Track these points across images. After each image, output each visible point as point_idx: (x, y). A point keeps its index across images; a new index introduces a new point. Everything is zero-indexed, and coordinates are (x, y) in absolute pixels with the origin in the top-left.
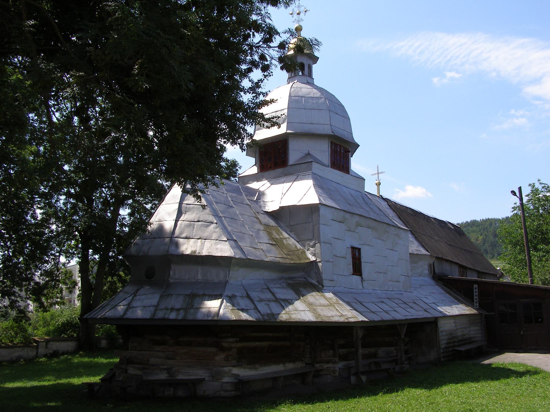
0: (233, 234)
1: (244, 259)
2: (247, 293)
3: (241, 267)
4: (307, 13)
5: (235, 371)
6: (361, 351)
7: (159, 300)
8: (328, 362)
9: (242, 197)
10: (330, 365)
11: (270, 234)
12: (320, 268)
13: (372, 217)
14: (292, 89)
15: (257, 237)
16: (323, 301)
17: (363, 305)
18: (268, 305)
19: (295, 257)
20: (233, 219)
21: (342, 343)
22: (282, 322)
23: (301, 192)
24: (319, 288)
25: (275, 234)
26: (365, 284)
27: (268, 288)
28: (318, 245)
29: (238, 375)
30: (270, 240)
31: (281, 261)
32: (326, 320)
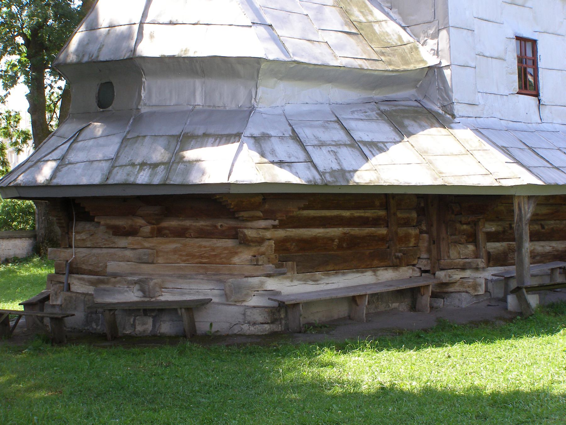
0: (266, 13)
1: (285, 62)
2: (293, 131)
3: (281, 79)
5: (272, 284)
6: (527, 246)
7: (120, 147)
8: (463, 268)
10: (468, 273)
15: (317, 20)
17: (538, 154)
18: (335, 153)
19: (396, 59)
21: (493, 229)
22: (358, 186)
24: (443, 118)
26: (545, 112)
27: (338, 121)
28: (443, 33)
29: (278, 293)
30: (346, 24)
31: (366, 65)
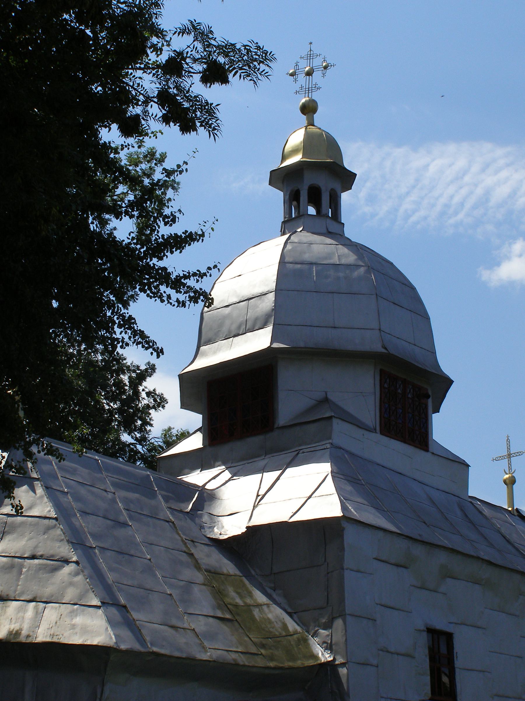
0: (120, 590)
9: (153, 502)
11: (219, 594)
12: (344, 680)
13: (482, 555)
14: (289, 247)
20: (124, 554)
23: (303, 492)
25: (232, 594)
30: (219, 607)
31: (242, 660)
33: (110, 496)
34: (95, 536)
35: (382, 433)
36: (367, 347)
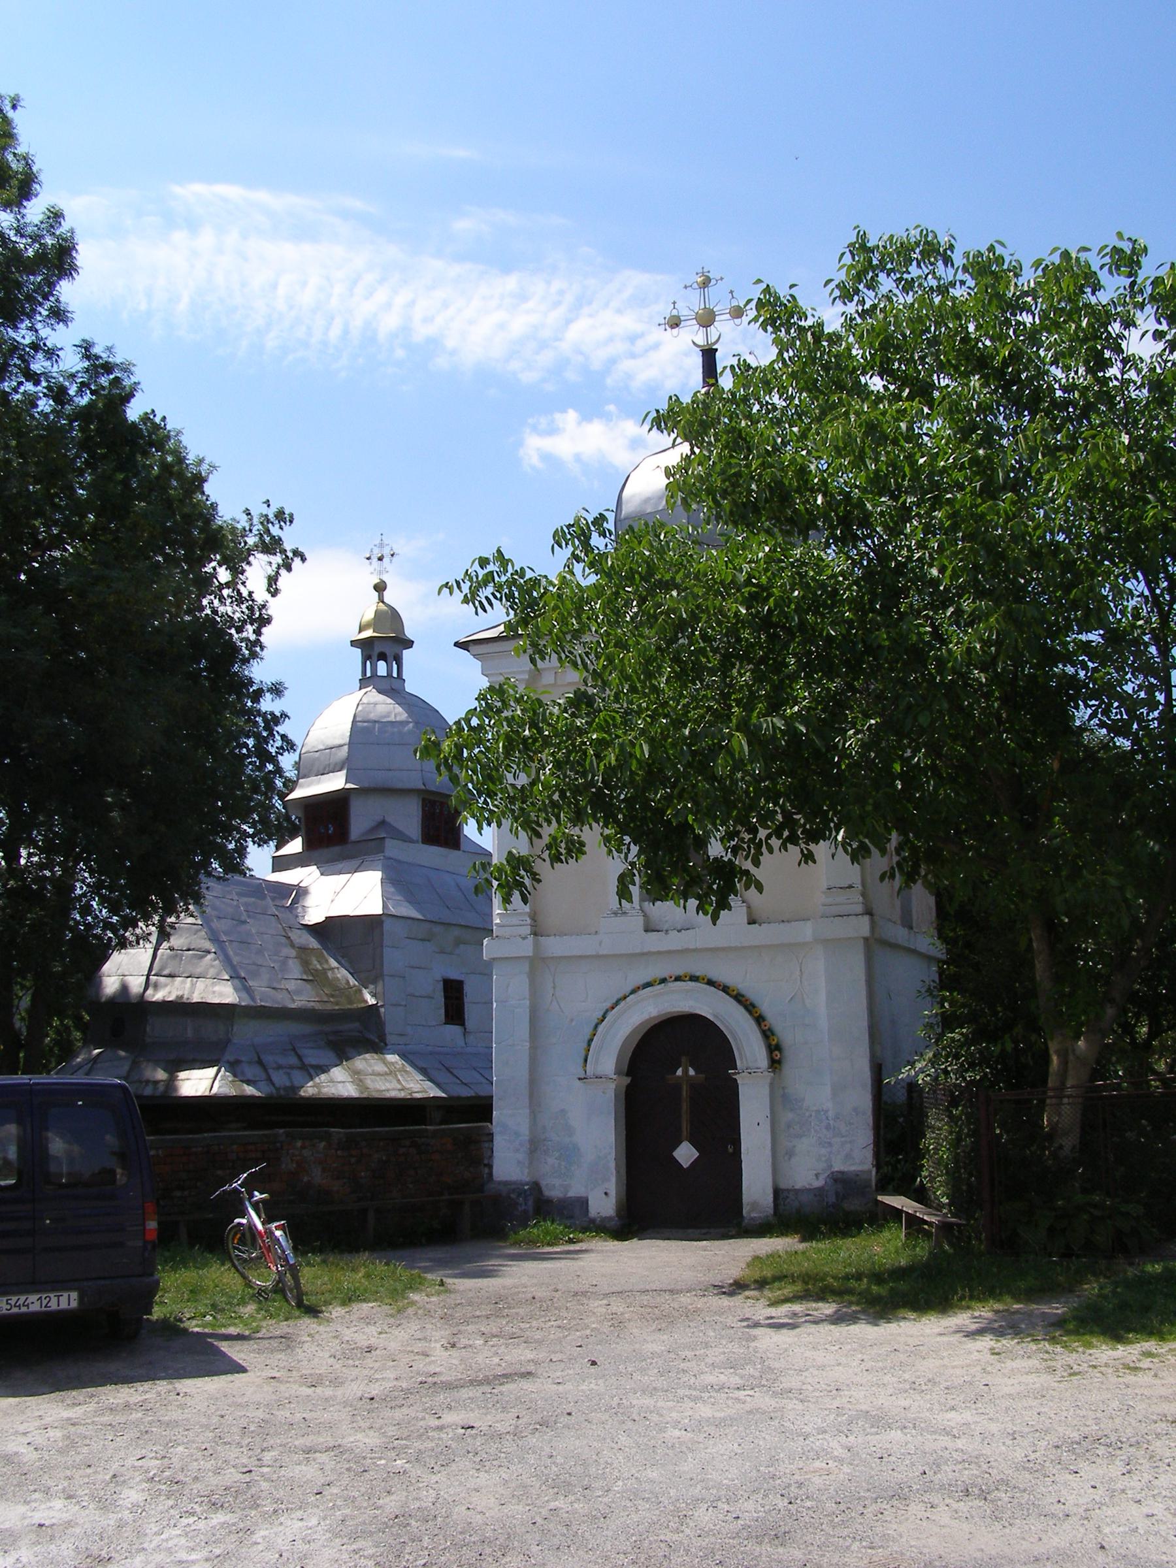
4: (395, 559)
11: (305, 964)
14: (360, 708)
16: (380, 1068)
18: (289, 1074)
22: (303, 1098)
24: (377, 1045)
26: (471, 1039)
27: (294, 1049)
30: (305, 973)
31: (318, 1006)
32: (376, 1095)
33: (235, 903)
34: (225, 934)
35: (423, 842)
36: (412, 785)
